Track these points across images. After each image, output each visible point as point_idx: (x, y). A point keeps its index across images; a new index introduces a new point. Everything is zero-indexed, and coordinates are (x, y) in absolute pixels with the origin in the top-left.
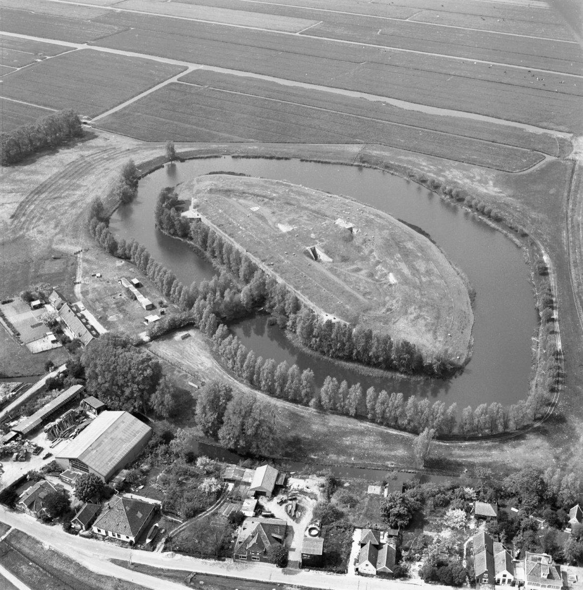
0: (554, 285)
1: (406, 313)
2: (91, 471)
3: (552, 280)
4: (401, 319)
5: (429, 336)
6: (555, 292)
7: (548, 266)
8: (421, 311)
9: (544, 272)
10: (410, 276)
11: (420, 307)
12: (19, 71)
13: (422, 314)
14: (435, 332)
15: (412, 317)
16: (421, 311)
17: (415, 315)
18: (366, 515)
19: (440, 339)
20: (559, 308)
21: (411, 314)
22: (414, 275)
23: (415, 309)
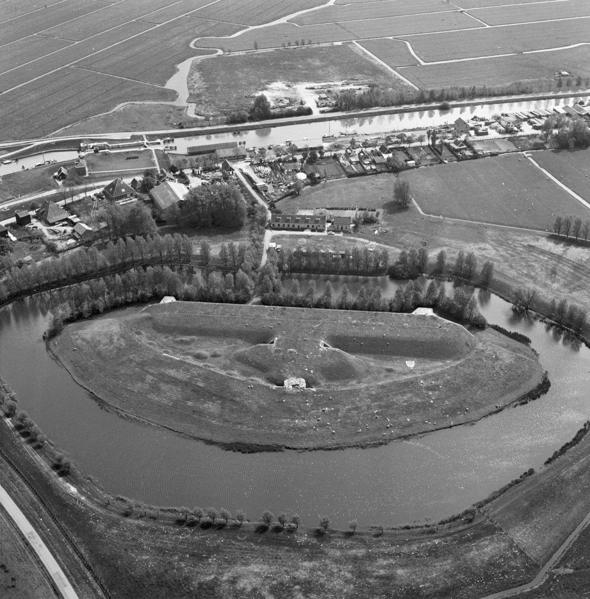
0: (36, 457)
1: (122, 336)
2: (155, 187)
3: (42, 463)
4: (119, 330)
5: (88, 337)
6: (28, 448)
7: (61, 479)
8: (115, 347)
9: (63, 470)
10: (163, 370)
11: (119, 349)
12: (488, 28)
13: (112, 346)
14: (88, 342)
15: (115, 338)
16: (115, 347)
17: (115, 341)
18: (20, 248)
19: (79, 341)
20: (11, 432)
21: (118, 339)
22: (162, 374)
23: (121, 345)
